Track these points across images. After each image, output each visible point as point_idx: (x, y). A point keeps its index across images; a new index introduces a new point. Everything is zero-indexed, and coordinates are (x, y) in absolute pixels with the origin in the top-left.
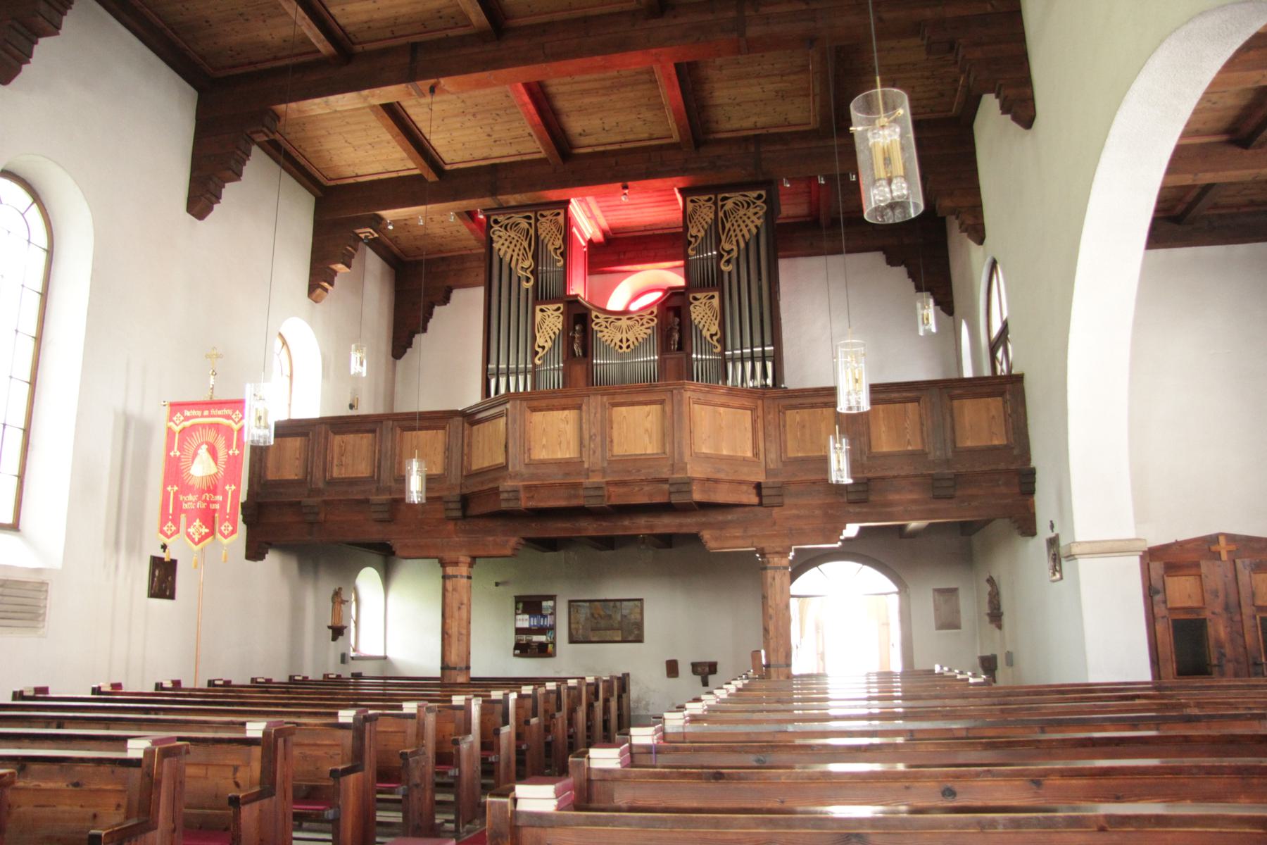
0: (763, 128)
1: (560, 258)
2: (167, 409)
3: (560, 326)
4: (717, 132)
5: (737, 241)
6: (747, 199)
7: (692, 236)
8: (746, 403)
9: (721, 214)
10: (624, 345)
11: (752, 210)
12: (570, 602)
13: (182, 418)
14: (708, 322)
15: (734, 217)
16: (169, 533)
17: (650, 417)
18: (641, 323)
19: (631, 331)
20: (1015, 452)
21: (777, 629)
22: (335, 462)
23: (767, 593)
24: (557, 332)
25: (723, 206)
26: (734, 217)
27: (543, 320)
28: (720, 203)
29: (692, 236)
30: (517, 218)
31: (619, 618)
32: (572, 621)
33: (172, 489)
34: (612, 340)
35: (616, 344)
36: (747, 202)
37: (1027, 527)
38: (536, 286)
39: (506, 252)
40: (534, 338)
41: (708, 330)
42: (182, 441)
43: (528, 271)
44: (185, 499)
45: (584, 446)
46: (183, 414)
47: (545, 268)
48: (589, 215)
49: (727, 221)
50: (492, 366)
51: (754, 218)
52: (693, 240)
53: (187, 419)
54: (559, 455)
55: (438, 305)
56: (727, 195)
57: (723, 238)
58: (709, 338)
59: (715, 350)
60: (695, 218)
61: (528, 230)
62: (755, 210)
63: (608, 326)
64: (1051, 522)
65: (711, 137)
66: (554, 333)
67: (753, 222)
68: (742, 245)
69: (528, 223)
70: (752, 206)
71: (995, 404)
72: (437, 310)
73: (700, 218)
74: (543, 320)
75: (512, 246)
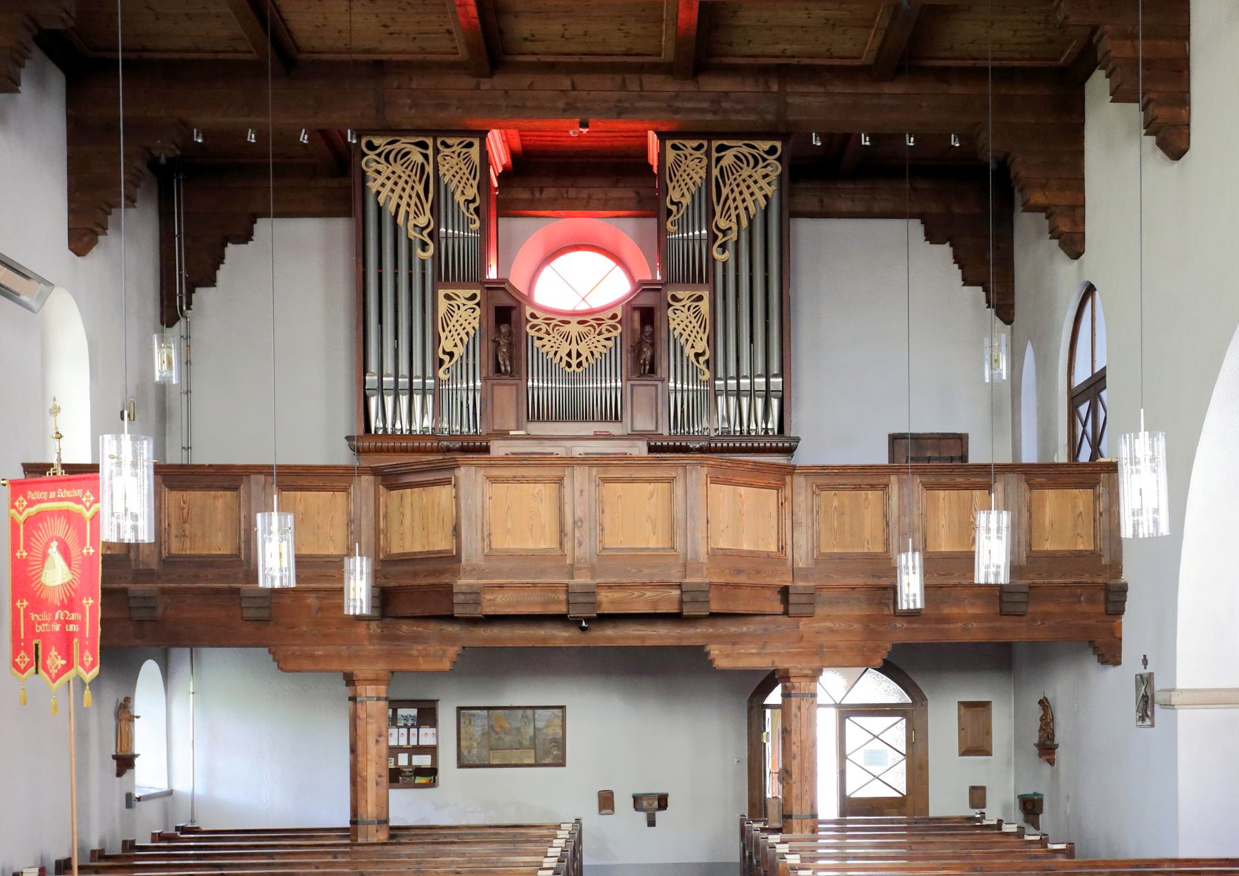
0: (794, 57)
1: (475, 217)
2: (8, 489)
3: (476, 324)
4: (726, 56)
5: (738, 216)
6: (754, 152)
7: (672, 203)
8: (772, 482)
9: (715, 172)
10: (574, 362)
11: (760, 171)
12: (460, 709)
13: (25, 503)
14: (693, 335)
15: (735, 179)
16: (22, 666)
17: (653, 500)
18: (597, 331)
19: (584, 341)
20: (1105, 561)
21: (802, 770)
22: (174, 531)
23: (791, 725)
24: (472, 333)
25: (719, 159)
26: (735, 179)
27: (450, 312)
28: (715, 155)
29: (672, 203)
30: (404, 144)
31: (515, 724)
32: (462, 736)
33: (23, 604)
34: (556, 353)
35: (561, 358)
36: (753, 156)
37: (1110, 654)
38: (437, 256)
39: (389, 198)
40: (437, 340)
41: (693, 347)
42: (28, 536)
43: (425, 232)
44: (38, 619)
45: (566, 535)
46: (25, 497)
47: (450, 231)
48: (505, 139)
49: (725, 185)
50: (372, 379)
51: (763, 183)
52: (674, 208)
53: (31, 503)
54: (530, 545)
55: (233, 243)
56: (725, 143)
57: (718, 209)
58: (692, 358)
59: (471, 226)
60: (678, 174)
61: (423, 165)
62: (765, 171)
63: (551, 332)
64: (1145, 656)
65: (716, 60)
66: (467, 334)
67: (761, 189)
68: (745, 223)
69: (422, 154)
70: (761, 164)
71: (1082, 497)
72: (231, 250)
73: (685, 176)
74: (450, 312)
75: (398, 190)
